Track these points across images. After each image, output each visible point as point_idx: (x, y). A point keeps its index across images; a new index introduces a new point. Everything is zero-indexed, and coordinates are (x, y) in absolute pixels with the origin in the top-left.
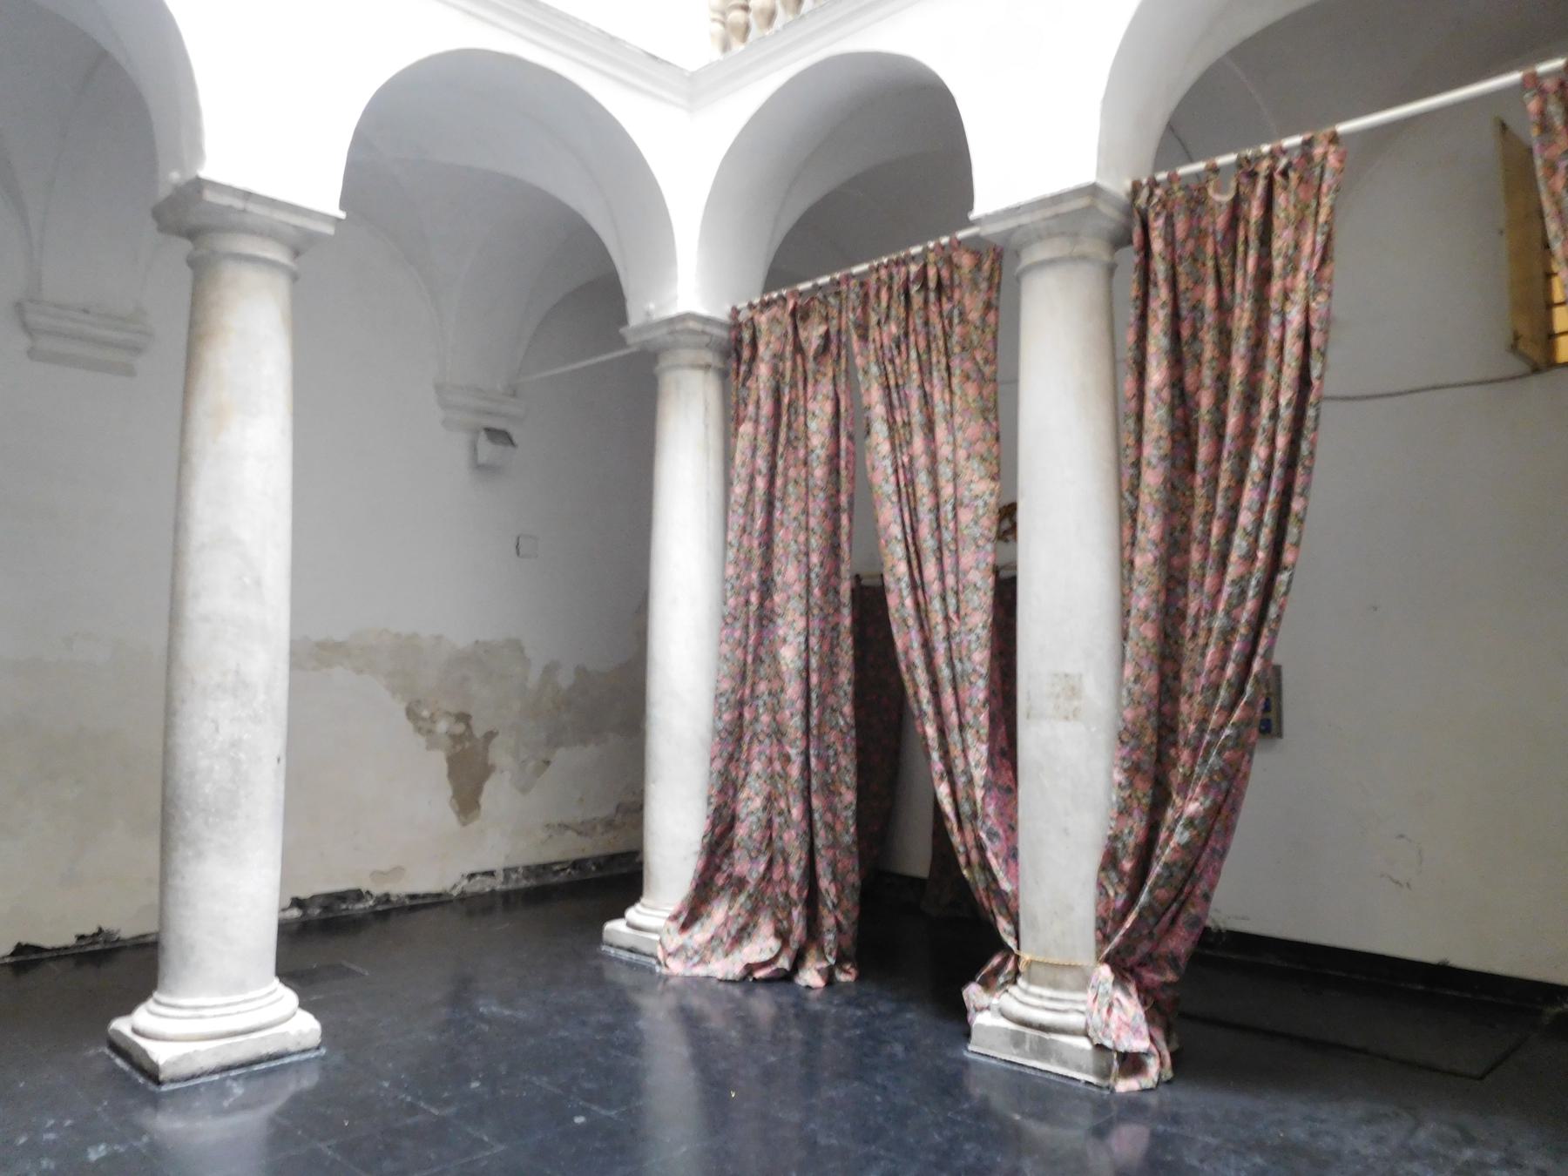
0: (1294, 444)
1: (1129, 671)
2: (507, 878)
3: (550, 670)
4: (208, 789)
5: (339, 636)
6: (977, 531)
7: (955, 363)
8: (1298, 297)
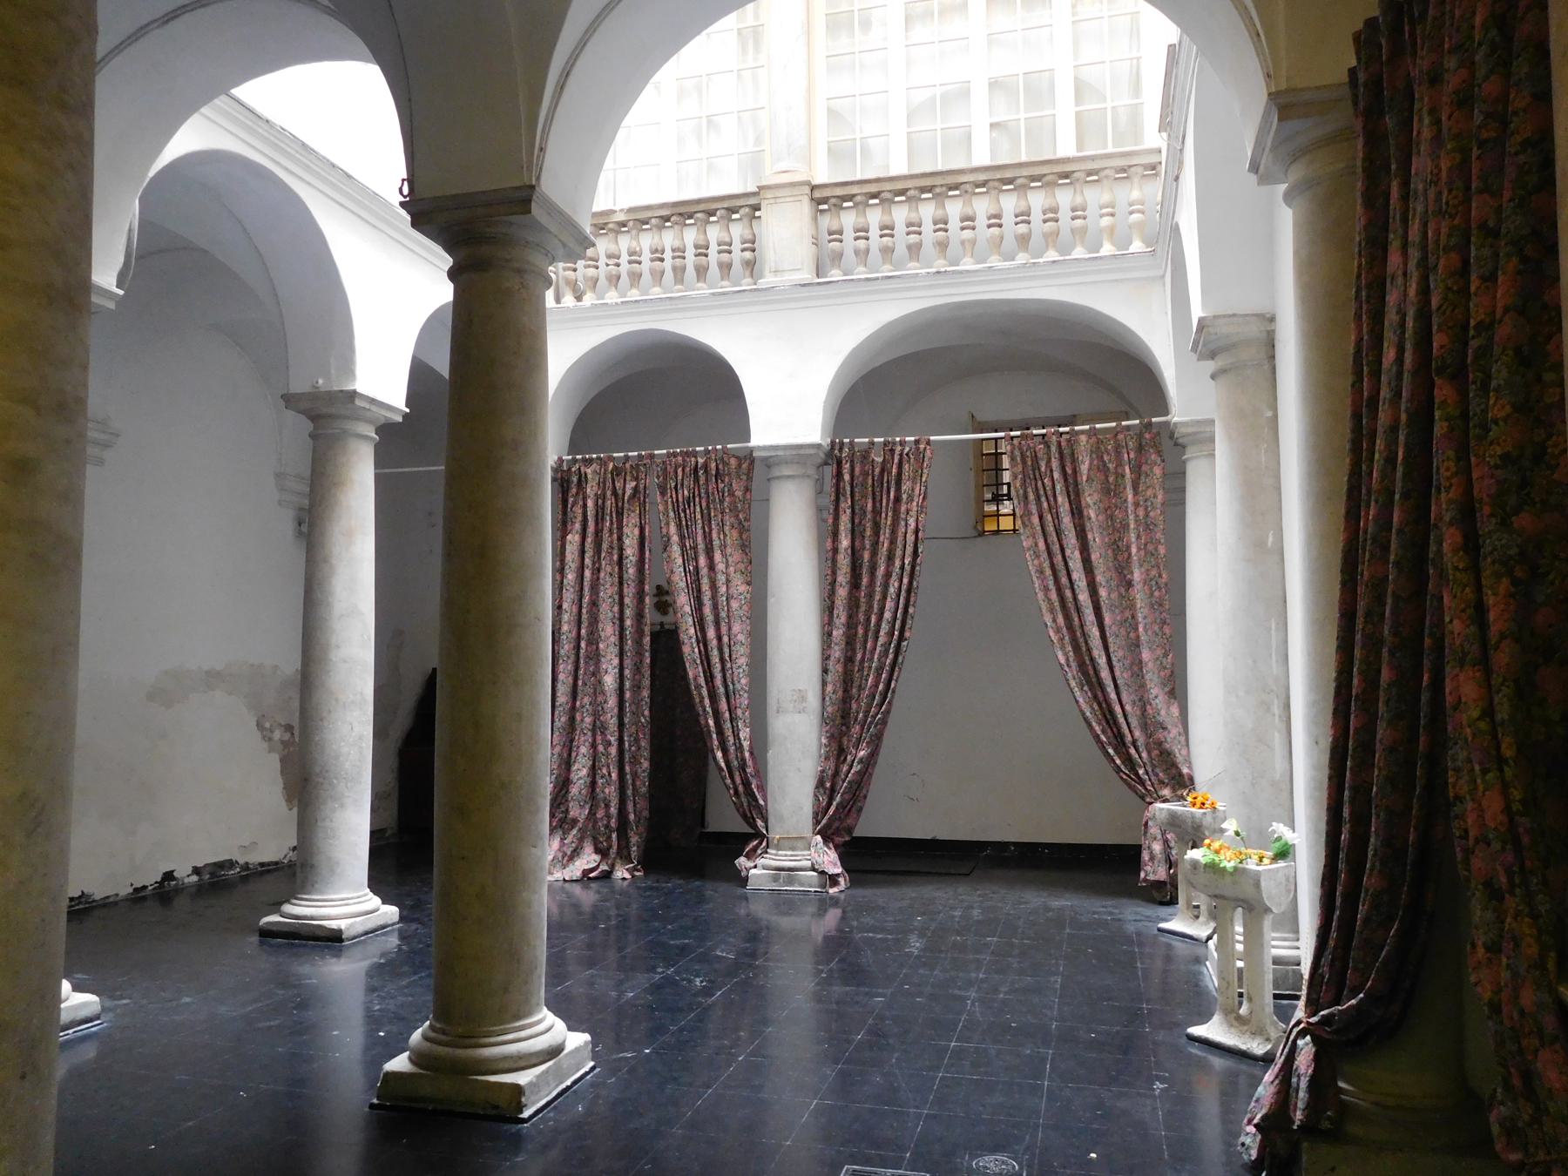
0: (910, 583)
4: (347, 765)
6: (741, 613)
8: (913, 513)
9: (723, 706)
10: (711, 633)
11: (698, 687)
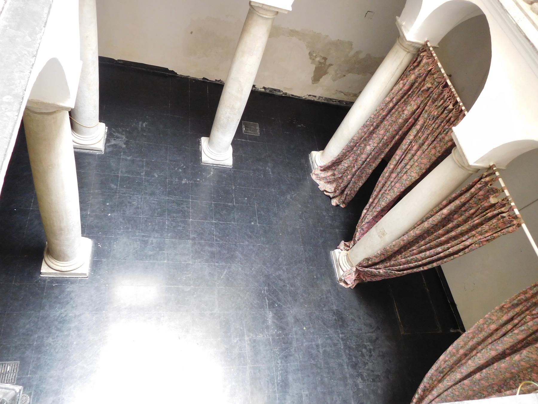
1: (394, 243)
3: (358, 53)
5: (298, 29)
7: (435, 142)
8: (475, 239)
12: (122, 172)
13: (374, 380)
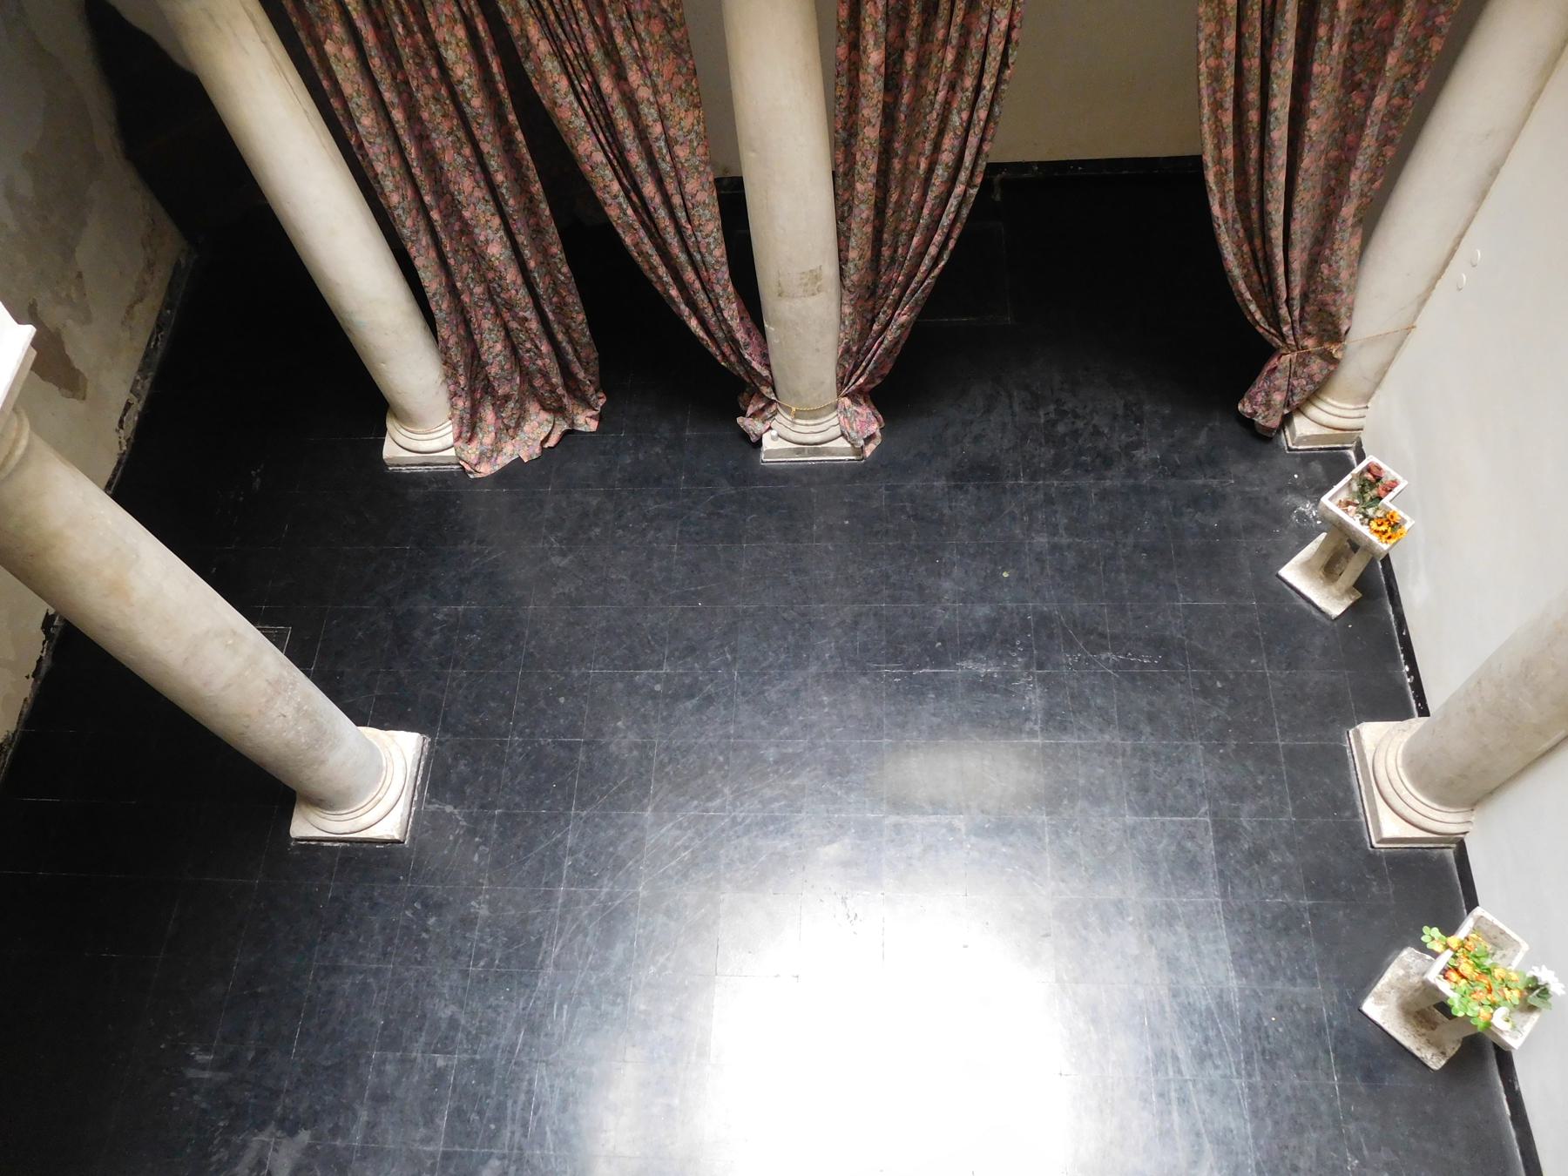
2: (137, 395)
9: (689, 275)
10: (649, 189)
11: (647, 256)
12: (427, 1140)
13: (1139, 420)
